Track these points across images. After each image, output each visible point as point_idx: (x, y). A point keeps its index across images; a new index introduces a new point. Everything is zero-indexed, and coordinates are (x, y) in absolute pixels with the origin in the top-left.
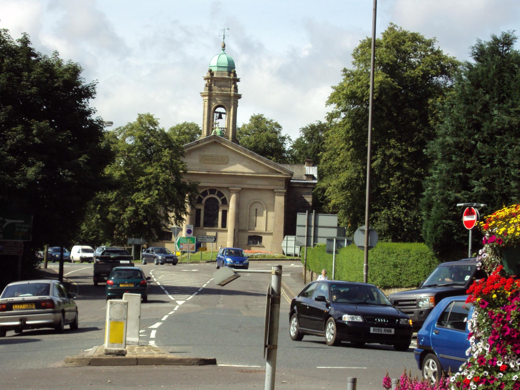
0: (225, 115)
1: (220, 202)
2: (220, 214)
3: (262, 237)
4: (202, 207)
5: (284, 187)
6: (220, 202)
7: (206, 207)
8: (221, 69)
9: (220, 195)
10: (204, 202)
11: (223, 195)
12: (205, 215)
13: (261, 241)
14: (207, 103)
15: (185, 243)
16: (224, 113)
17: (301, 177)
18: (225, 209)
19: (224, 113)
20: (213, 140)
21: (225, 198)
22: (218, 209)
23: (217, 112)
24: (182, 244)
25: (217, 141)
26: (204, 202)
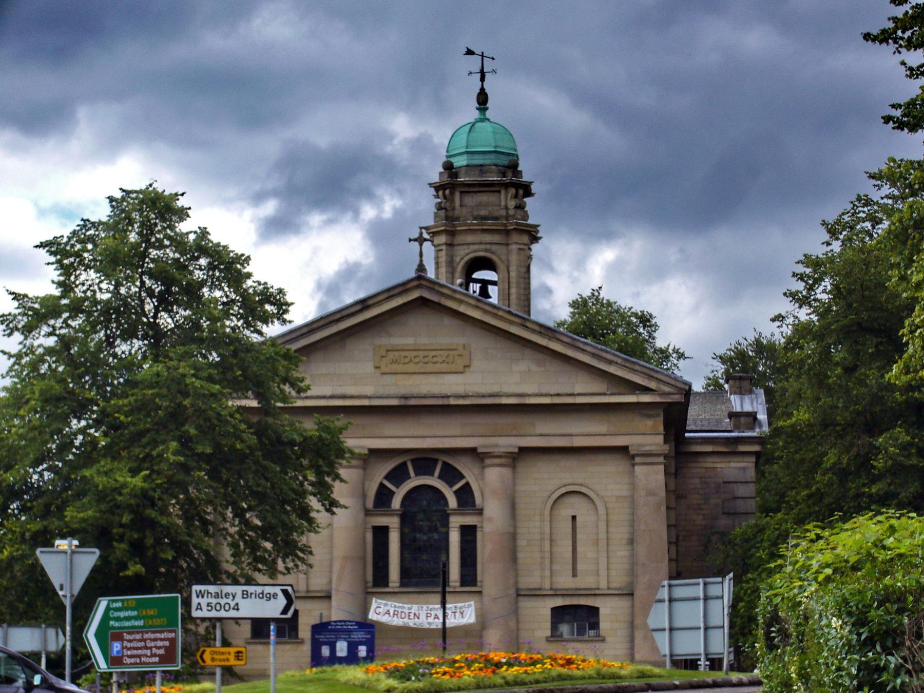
0: (496, 288)
1: (453, 502)
2: (454, 537)
3: (597, 609)
4: (393, 522)
5: (660, 439)
6: (453, 502)
7: (405, 518)
8: (478, 160)
9: (451, 475)
10: (396, 503)
11: (462, 477)
12: (404, 546)
13: (595, 625)
14: (443, 254)
15: (132, 630)
16: (494, 283)
17: (719, 421)
18: (469, 520)
19: (494, 283)
20: (415, 295)
21: (467, 484)
22: (446, 525)
23: (477, 281)
24: (118, 637)
25: (427, 295)
26: (396, 503)
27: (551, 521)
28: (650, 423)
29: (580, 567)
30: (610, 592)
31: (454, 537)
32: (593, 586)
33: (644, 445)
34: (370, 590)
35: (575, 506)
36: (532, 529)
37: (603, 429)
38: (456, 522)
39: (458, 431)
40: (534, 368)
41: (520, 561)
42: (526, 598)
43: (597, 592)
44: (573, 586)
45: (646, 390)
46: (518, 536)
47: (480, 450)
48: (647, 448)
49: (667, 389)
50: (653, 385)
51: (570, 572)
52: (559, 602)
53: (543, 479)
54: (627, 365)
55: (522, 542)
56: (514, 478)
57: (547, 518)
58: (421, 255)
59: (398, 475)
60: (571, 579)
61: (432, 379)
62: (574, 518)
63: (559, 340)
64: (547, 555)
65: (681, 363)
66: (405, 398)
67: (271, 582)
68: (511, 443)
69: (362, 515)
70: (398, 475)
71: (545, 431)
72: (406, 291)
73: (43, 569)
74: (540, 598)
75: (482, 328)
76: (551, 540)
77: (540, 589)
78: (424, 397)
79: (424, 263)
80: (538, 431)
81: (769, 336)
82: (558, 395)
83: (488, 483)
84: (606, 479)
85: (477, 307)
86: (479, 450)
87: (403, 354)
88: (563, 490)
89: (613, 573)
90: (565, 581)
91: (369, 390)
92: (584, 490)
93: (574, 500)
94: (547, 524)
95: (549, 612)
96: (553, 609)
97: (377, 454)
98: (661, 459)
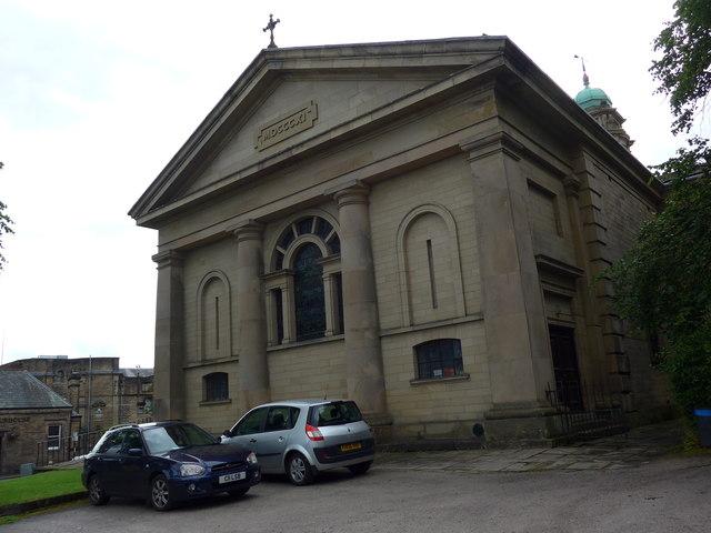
4: (282, 283)
6: (325, 253)
10: (286, 264)
27: (406, 251)
29: (439, 296)
30: (468, 319)
31: (328, 286)
32: (453, 315)
35: (426, 230)
36: (388, 264)
38: (328, 270)
42: (389, 340)
43: (455, 321)
44: (434, 318)
46: (377, 275)
49: (484, 58)
50: (467, 61)
52: (420, 339)
53: (392, 210)
54: (437, 49)
55: (380, 280)
56: (368, 215)
57: (401, 248)
59: (286, 240)
62: (429, 242)
63: (371, 55)
64: (404, 288)
69: (256, 281)
70: (286, 240)
73: (60, 366)
76: (407, 272)
81: (679, 156)
84: (450, 192)
85: (306, 58)
89: (470, 296)
90: (425, 314)
95: (411, 352)
96: (204, 377)
98: (500, 146)
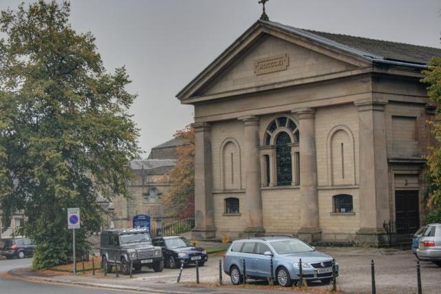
4: (270, 152)
10: (272, 142)
20: (260, 32)
26: (272, 142)
28: (365, 86)
33: (361, 100)
34: (262, 188)
37: (344, 92)
39: (285, 102)
40: (314, 62)
41: (264, 207)
44: (342, 183)
45: (356, 68)
47: (293, 111)
48: (363, 101)
49: (364, 65)
50: (357, 64)
51: (341, 176)
57: (329, 145)
58: (264, 9)
59: (272, 127)
60: (342, 179)
61: (276, 75)
65: (139, 132)
66: (258, 87)
67: (244, 176)
68: (304, 106)
71: (320, 98)
72: (256, 30)
74: (327, 191)
75: (326, 37)
77: (326, 186)
78: (287, 82)
79: (267, 13)
80: (317, 98)
82: (317, 76)
83: (302, 125)
86: (292, 111)
87: (264, 63)
88: (334, 131)
90: (338, 181)
91: (253, 84)
92: (338, 128)
93: (340, 135)
94: (329, 149)
97: (258, 119)
